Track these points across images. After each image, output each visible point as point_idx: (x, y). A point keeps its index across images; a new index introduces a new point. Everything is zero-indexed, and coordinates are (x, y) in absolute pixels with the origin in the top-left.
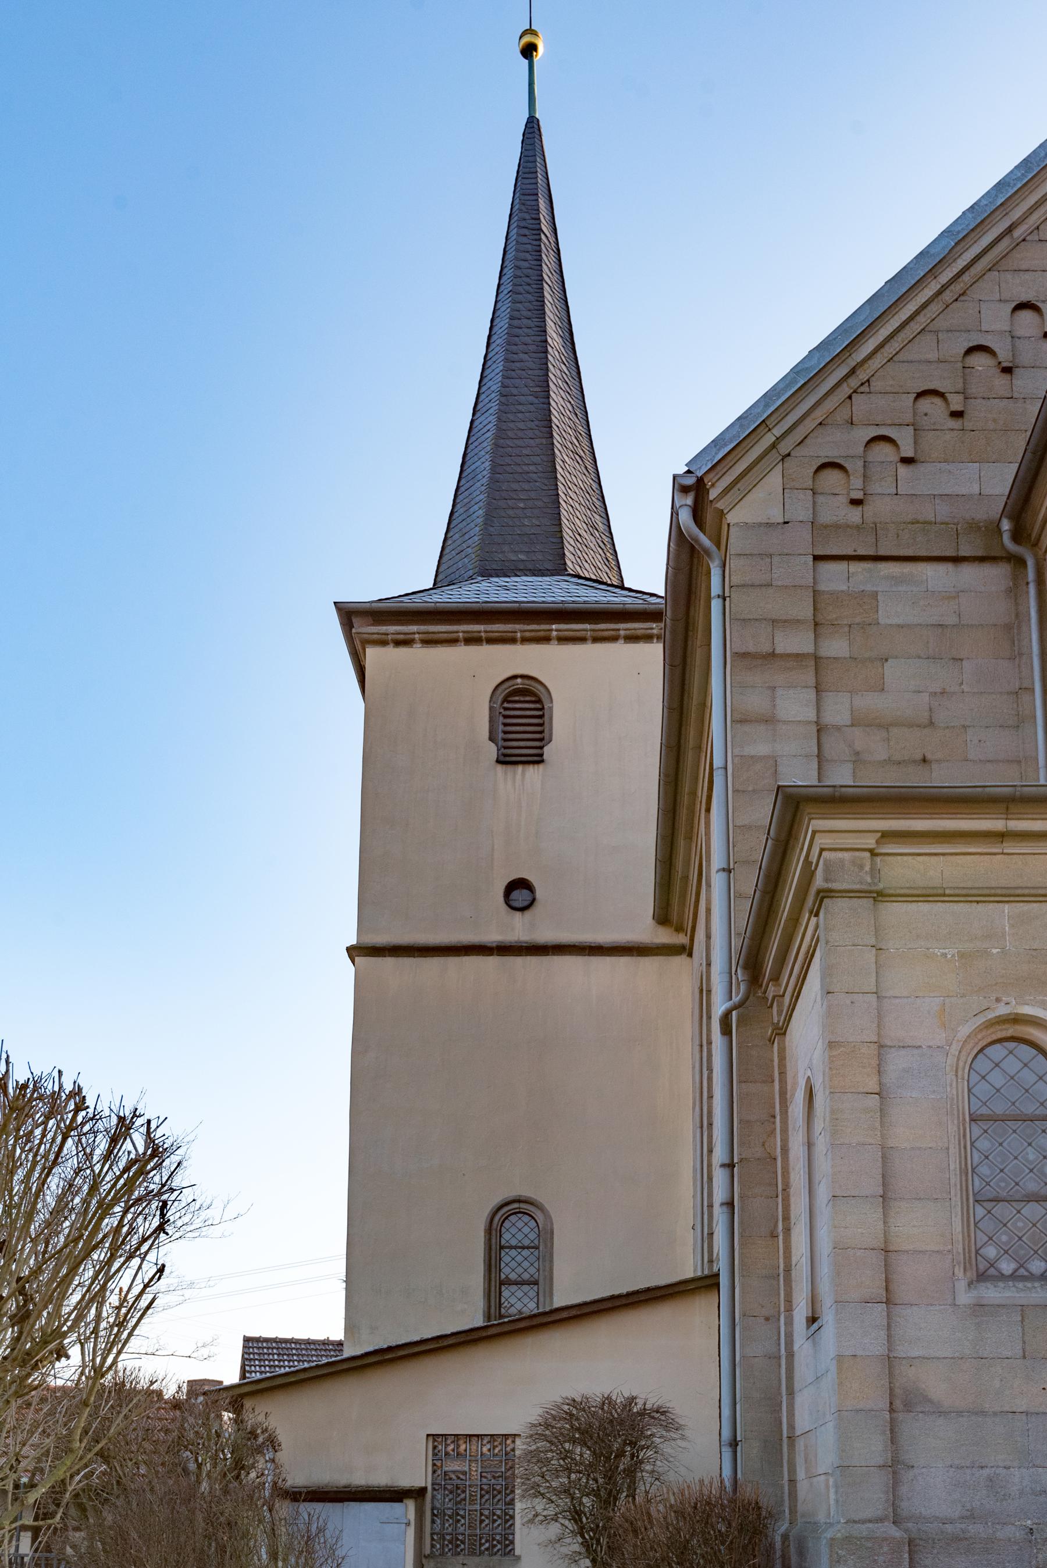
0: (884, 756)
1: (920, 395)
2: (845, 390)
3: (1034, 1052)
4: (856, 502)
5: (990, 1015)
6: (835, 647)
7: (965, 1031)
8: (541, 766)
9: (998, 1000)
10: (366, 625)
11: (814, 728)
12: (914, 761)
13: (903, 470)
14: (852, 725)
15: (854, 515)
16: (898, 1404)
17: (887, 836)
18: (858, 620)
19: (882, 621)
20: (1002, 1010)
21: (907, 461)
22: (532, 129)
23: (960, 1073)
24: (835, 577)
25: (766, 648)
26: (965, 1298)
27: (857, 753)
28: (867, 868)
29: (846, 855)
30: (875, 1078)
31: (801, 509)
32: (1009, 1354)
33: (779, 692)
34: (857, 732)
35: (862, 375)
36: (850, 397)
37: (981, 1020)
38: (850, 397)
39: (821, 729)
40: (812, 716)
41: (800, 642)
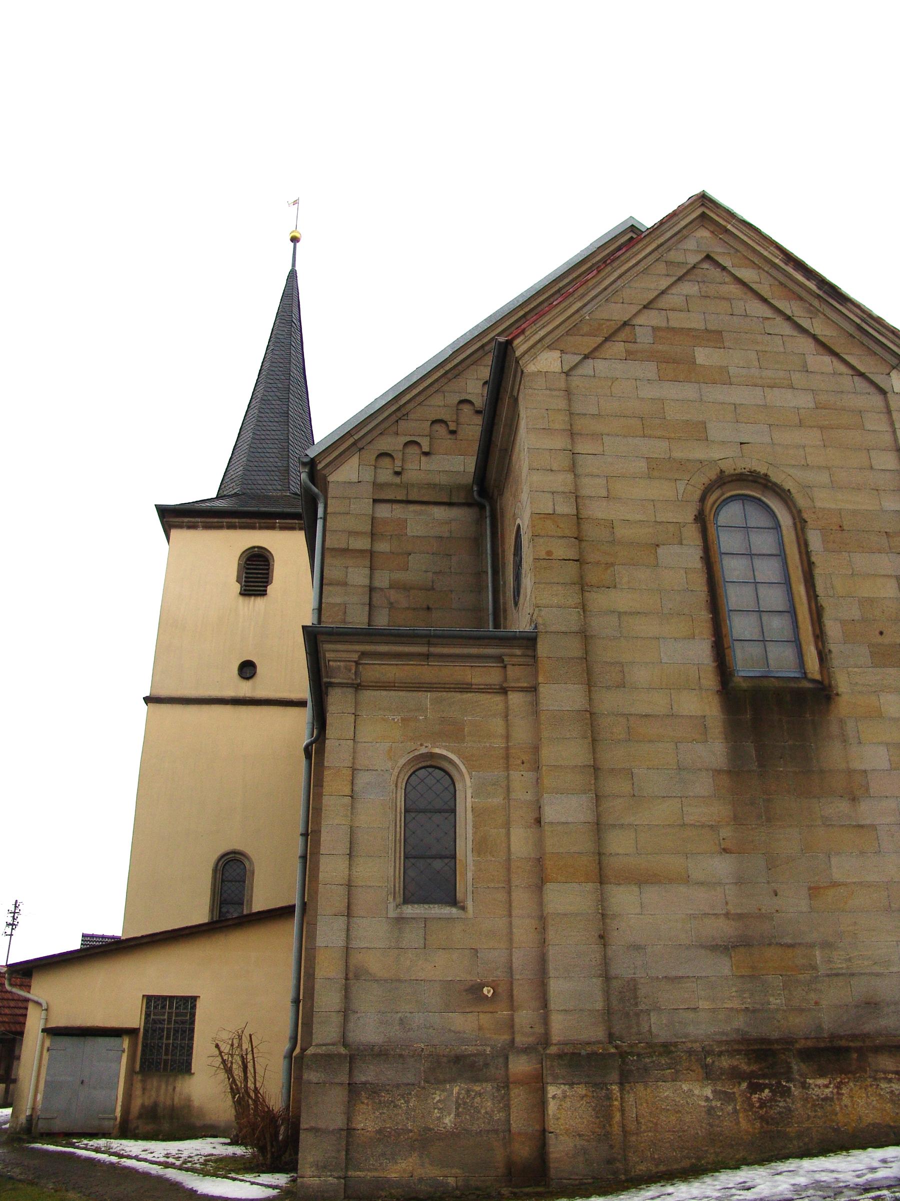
0: (407, 605)
1: (434, 422)
2: (394, 418)
3: (443, 773)
4: (398, 474)
5: (417, 753)
6: (383, 547)
7: (402, 761)
8: (265, 598)
9: (421, 745)
10: (173, 517)
11: (367, 589)
12: (423, 609)
13: (423, 458)
14: (390, 588)
15: (397, 480)
16: (351, 975)
17: (363, 654)
18: (396, 533)
19: (409, 533)
20: (423, 750)
21: (426, 454)
22: (292, 277)
23: (399, 785)
24: (384, 512)
25: (344, 546)
26: (392, 914)
27: (391, 604)
28: (353, 671)
29: (342, 664)
30: (349, 787)
31: (368, 476)
32: (416, 946)
33: (350, 570)
34: (392, 592)
35: (404, 411)
36: (397, 421)
37: (412, 755)
38: (397, 421)
39: (372, 589)
40: (367, 582)
41: (362, 543)
